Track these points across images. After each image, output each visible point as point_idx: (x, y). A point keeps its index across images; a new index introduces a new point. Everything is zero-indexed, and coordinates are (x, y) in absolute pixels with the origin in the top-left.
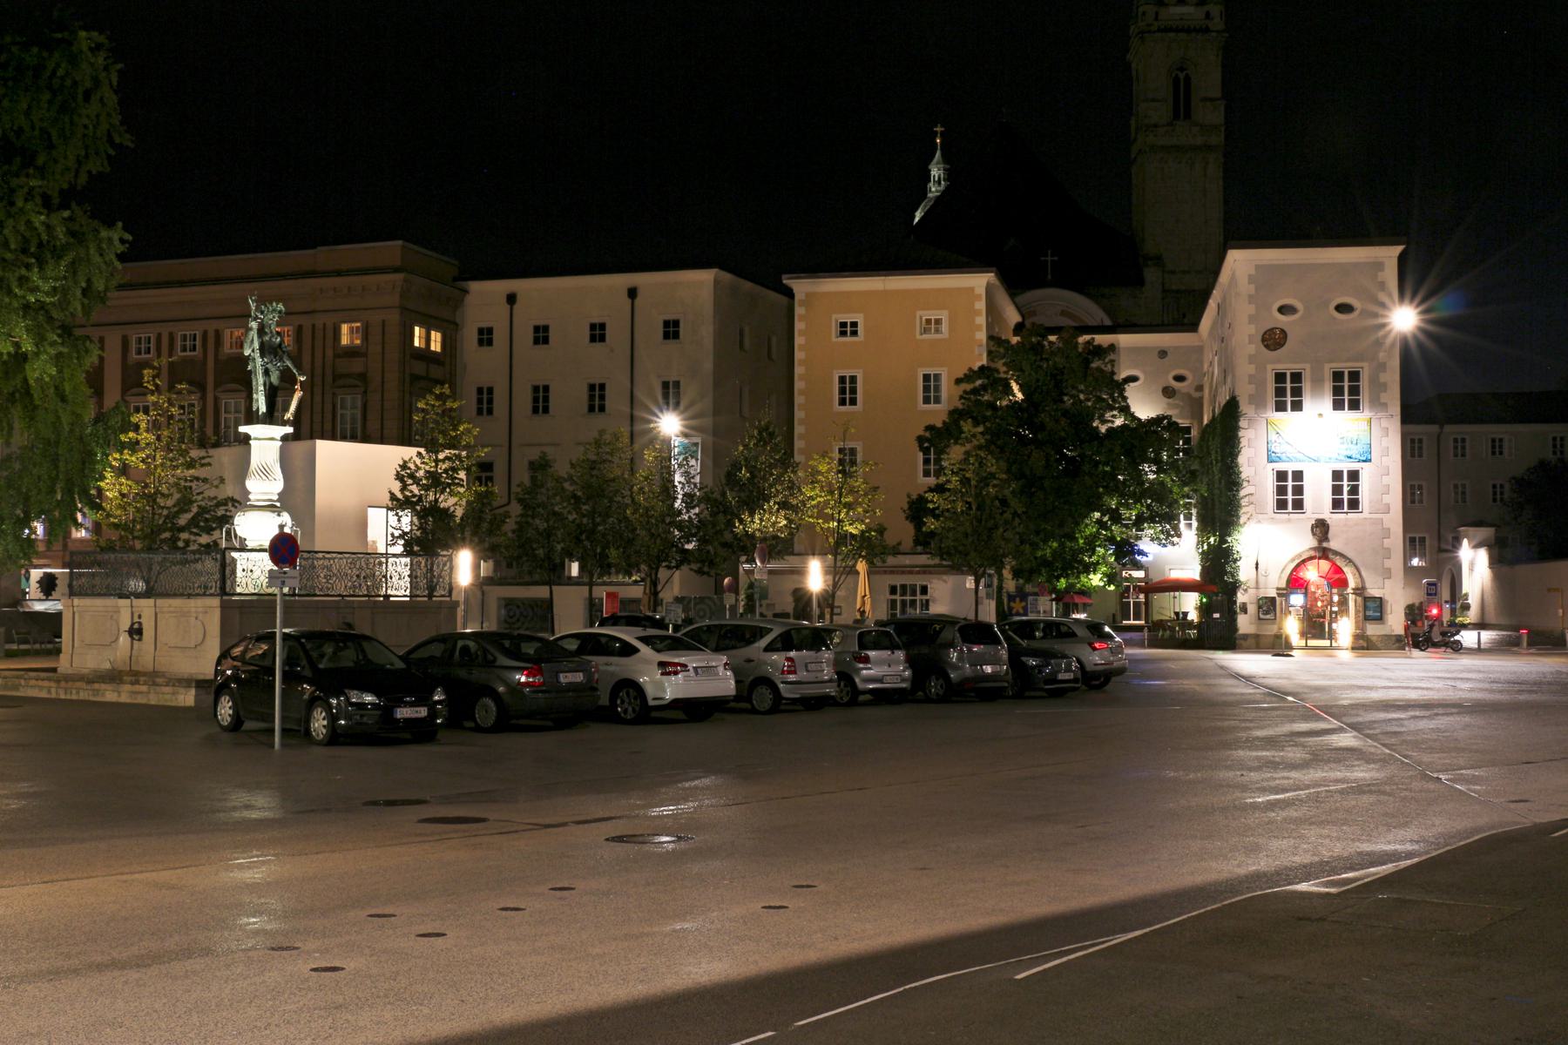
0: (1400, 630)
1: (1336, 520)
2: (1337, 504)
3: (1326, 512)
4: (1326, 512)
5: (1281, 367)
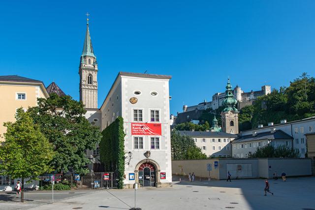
2: (153, 147)
3: (149, 149)
4: (149, 149)
5: (136, 108)
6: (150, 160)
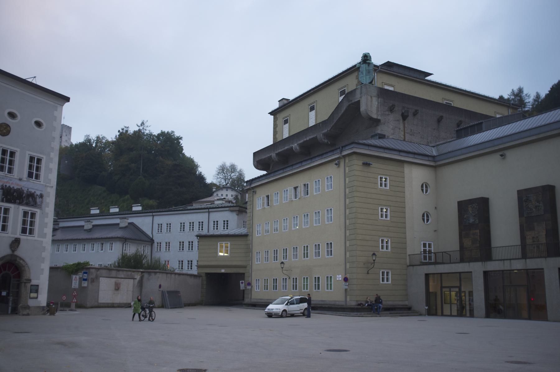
0: (44, 304)
1: (23, 237)
4: (18, 234)
5: (6, 147)
6: (16, 256)
